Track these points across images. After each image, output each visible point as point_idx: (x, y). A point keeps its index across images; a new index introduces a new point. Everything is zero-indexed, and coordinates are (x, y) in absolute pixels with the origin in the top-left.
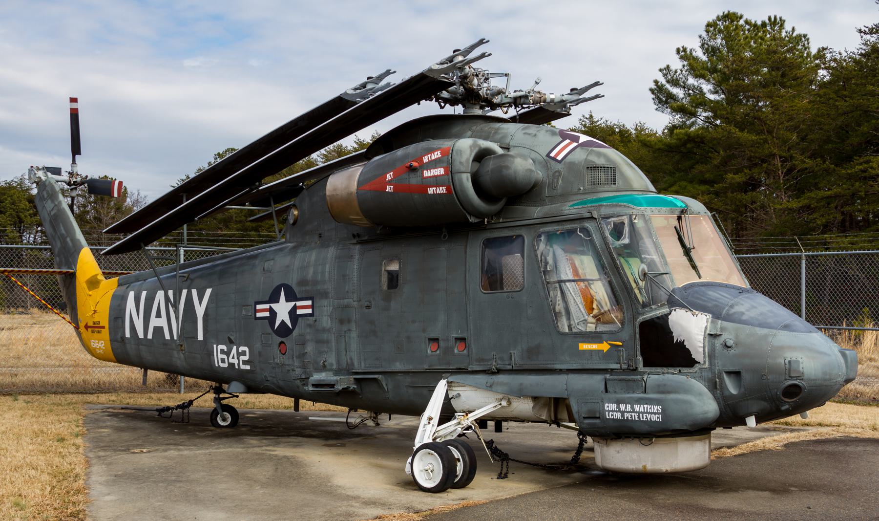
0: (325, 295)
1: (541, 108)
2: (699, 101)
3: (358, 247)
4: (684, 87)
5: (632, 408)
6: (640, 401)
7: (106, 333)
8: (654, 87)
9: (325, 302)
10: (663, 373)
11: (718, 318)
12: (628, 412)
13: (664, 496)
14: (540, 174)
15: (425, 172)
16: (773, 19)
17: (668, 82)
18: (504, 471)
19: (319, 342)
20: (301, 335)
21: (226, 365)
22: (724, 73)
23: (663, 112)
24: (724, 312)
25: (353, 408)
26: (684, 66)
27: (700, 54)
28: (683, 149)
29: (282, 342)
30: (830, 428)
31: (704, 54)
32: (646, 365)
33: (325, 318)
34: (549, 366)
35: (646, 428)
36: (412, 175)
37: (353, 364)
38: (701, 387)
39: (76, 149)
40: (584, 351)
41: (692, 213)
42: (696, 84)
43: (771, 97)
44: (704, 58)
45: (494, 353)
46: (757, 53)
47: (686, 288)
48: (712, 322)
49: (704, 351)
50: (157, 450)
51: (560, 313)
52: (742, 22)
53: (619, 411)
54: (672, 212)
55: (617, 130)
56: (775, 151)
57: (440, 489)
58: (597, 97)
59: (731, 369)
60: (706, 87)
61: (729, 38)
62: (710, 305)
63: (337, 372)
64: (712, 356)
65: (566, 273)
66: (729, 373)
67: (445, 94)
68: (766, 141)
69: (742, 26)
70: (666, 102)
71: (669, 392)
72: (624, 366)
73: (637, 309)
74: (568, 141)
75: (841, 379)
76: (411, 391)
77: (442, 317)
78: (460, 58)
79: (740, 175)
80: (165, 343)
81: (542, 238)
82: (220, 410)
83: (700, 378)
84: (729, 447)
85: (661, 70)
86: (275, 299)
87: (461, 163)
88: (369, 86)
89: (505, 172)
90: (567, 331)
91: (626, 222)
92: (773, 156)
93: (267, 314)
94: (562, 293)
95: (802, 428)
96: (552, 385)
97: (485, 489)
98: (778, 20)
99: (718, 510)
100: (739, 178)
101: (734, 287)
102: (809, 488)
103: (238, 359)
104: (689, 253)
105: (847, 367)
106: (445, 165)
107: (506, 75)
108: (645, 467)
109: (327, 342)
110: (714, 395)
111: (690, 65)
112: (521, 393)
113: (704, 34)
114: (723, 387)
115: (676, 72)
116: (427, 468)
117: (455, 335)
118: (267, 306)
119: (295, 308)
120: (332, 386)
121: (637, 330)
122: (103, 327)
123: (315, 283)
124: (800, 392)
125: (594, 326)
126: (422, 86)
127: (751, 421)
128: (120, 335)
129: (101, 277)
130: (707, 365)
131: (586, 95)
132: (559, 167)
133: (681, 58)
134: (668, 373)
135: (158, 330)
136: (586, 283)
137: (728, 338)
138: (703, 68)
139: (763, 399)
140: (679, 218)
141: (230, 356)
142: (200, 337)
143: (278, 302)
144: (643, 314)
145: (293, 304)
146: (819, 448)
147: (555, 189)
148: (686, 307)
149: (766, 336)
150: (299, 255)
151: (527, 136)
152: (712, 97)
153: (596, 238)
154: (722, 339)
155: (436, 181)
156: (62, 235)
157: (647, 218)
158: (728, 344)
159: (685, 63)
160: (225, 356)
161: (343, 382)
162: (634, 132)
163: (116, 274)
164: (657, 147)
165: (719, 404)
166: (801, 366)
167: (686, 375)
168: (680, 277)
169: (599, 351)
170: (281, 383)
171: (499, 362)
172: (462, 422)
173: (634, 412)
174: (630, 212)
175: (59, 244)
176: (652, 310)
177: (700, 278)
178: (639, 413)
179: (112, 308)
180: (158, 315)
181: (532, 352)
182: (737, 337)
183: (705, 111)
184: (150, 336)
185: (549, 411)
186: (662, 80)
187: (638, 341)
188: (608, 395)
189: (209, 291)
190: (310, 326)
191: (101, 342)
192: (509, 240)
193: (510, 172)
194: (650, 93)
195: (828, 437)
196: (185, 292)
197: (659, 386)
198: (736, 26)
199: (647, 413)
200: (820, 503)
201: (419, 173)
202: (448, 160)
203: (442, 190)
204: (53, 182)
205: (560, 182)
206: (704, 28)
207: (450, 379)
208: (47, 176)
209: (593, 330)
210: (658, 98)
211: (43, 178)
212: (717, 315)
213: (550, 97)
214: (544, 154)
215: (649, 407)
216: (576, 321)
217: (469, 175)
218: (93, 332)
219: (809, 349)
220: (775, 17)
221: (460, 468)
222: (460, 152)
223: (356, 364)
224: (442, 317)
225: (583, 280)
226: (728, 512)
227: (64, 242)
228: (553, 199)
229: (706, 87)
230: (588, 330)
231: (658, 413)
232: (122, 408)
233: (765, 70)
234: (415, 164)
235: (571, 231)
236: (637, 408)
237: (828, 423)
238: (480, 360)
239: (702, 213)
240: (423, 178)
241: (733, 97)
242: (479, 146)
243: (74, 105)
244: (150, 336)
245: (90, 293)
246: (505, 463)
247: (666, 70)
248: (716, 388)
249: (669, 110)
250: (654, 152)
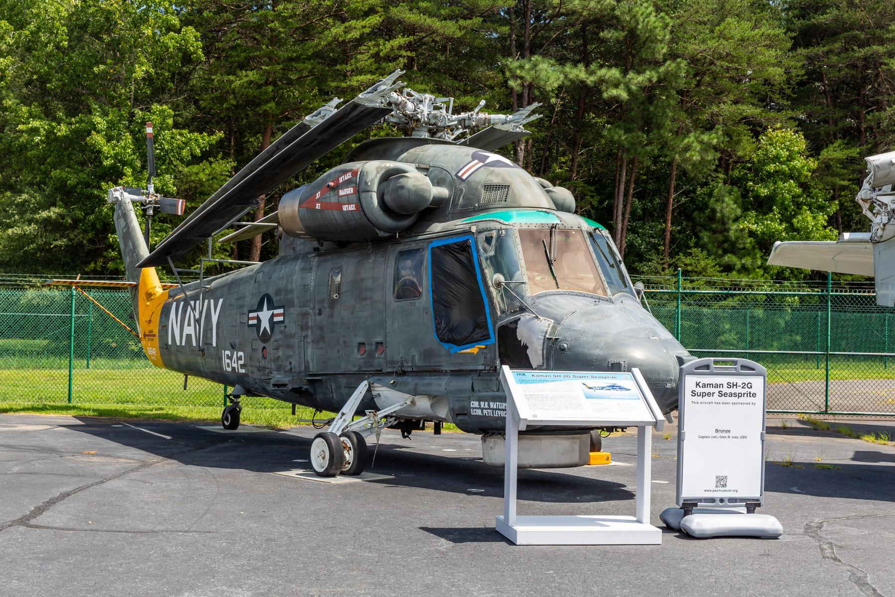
3: (317, 258)
5: (489, 405)
7: (157, 339)
9: (292, 310)
21: (229, 369)
29: (264, 348)
57: (327, 474)
86: (260, 308)
89: (404, 192)
93: (255, 322)
119: (273, 315)
120: (285, 385)
122: (155, 336)
135: (189, 337)
142: (214, 345)
160: (229, 361)
173: (489, 409)
180: (189, 325)
184: (183, 344)
189: (221, 300)
203: (352, 207)
211: (120, 198)
214: (453, 174)
240: (339, 197)
244: (183, 344)
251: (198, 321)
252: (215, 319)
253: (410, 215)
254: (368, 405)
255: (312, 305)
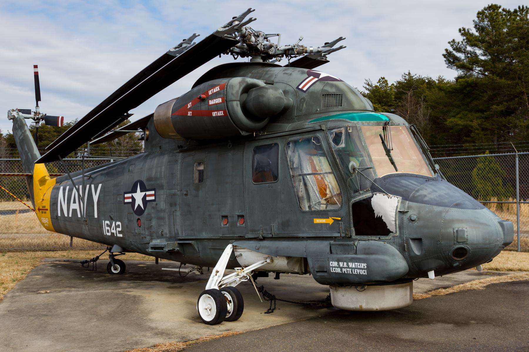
0: (162, 187)
1: (306, 57)
2: (474, 60)
3: (181, 154)
4: (465, 53)
5: (348, 265)
6: (353, 260)
7: (48, 212)
8: (445, 53)
9: (162, 192)
10: (368, 240)
11: (407, 200)
12: (345, 268)
13: (373, 329)
14: (290, 100)
15: (210, 101)
16: (521, 8)
17: (454, 49)
18: (273, 307)
19: (160, 218)
20: (149, 214)
21: (109, 234)
22: (489, 43)
23: (451, 68)
24: (411, 195)
25: (183, 263)
26: (464, 40)
27: (474, 31)
28: (465, 91)
29: (139, 219)
30: (525, 273)
31: (477, 31)
32: (356, 234)
33: (162, 202)
34: (296, 235)
35: (357, 280)
36: (202, 104)
37: (178, 233)
38: (394, 249)
39: (38, 98)
40: (318, 224)
41: (393, 124)
42: (472, 50)
43: (519, 57)
44: (477, 34)
45: (261, 226)
46: (510, 29)
47: (385, 178)
48: (402, 202)
49: (396, 223)
50: (55, 291)
51: (303, 197)
52: (500, 10)
53: (339, 267)
54: (378, 124)
55: (427, 81)
56: (524, 90)
57: (216, 321)
58: (341, 48)
59: (415, 236)
60: (479, 52)
61: (492, 20)
62: (401, 190)
63: (170, 239)
64: (401, 227)
65: (307, 169)
66: (414, 240)
67: (237, 50)
68: (517, 84)
69: (500, 12)
70: (453, 62)
71: (372, 254)
72: (343, 235)
73: (350, 194)
74: (312, 77)
75: (500, 243)
76: (212, 251)
77: (229, 201)
78: (237, 23)
79: (500, 106)
80: (78, 220)
81: (291, 145)
82: (112, 263)
83: (394, 244)
84: (445, 288)
85: (449, 43)
87: (232, 94)
88: (184, 46)
90: (307, 209)
91: (343, 132)
92: (523, 93)
93: (130, 200)
94: (305, 185)
95: (507, 272)
96: (298, 248)
97: (254, 319)
98: (525, 8)
99: (405, 341)
100: (500, 108)
101: (422, 177)
102: (484, 321)
103: (116, 230)
104: (395, 153)
105: (504, 233)
106: (222, 96)
107: (278, 35)
108: (361, 306)
109: (163, 218)
110: (403, 255)
111: (467, 39)
112: (277, 254)
113: (476, 19)
114: (410, 249)
115: (459, 43)
116: (206, 307)
117: (237, 213)
118: (130, 195)
119: (145, 196)
120: (162, 248)
121: (351, 208)
122: (47, 210)
123: (156, 179)
124: (466, 254)
125: (325, 206)
126: (215, 44)
127: (432, 274)
128: (55, 215)
129: (47, 178)
130: (398, 234)
131: (335, 47)
132: (304, 95)
133: (462, 34)
134: (372, 240)
135: (74, 211)
136: (321, 175)
137: (413, 214)
138: (476, 40)
139: (439, 258)
140: (384, 129)
141: (112, 229)
142: (96, 216)
143: (136, 192)
144: (354, 197)
145: (144, 193)
146: (510, 288)
147: (301, 110)
148: (384, 192)
149: (441, 212)
150: (148, 161)
151: (285, 75)
152: (483, 58)
153: (324, 144)
154: (408, 215)
155: (217, 108)
156: (26, 151)
157: (358, 129)
158: (413, 219)
159: (465, 38)
160: (109, 228)
161: (173, 245)
162: (437, 82)
163: (56, 175)
164: (447, 90)
165: (407, 262)
166: (466, 234)
167: (384, 241)
168: (382, 170)
169: (326, 224)
170: (140, 246)
171: (264, 232)
172: (240, 274)
174: (346, 124)
175: (24, 158)
176: (360, 194)
177: (397, 171)
178: (352, 268)
179: (51, 198)
180: (74, 202)
181: (285, 225)
182: (419, 213)
183: (479, 67)
184: (70, 216)
185: (301, 266)
186: (450, 49)
187: (351, 217)
188: (332, 255)
189: (100, 185)
190: (153, 208)
191: (47, 219)
192: (270, 146)
193: (265, 99)
194: (443, 57)
195: (521, 279)
196: (88, 186)
197: (365, 249)
198: (497, 13)
199: (357, 268)
200: (482, 334)
201: (206, 102)
202: (223, 93)
203: (221, 113)
204: (22, 118)
205: (304, 105)
206: (476, 15)
207: (235, 244)
208: (18, 115)
209: (324, 208)
210: (448, 60)
211: (16, 116)
212: (406, 197)
213: (309, 49)
214: (295, 87)
215: (358, 264)
216: (314, 203)
217: (238, 103)
218: (42, 213)
219: (475, 220)
220: (523, 7)
221: (230, 307)
222: (232, 87)
223: (180, 233)
224: (229, 201)
225: (319, 174)
226: (412, 342)
227: (27, 156)
228: (300, 118)
229: (479, 52)
230: (321, 209)
231: (364, 269)
232: (64, 261)
233: (516, 39)
234: (203, 96)
235: (309, 139)
236: (350, 265)
237: (526, 269)
238: (253, 231)
239: (401, 124)
241: (495, 59)
242: (247, 82)
243: (36, 70)
244: (70, 216)
245: (41, 188)
246: (273, 301)
247: (453, 42)
248: (405, 251)
249: (455, 67)
250: (446, 93)
251: (81, 199)
252: (96, 198)
253: (263, 119)
254: (233, 264)
255: (179, 188)
